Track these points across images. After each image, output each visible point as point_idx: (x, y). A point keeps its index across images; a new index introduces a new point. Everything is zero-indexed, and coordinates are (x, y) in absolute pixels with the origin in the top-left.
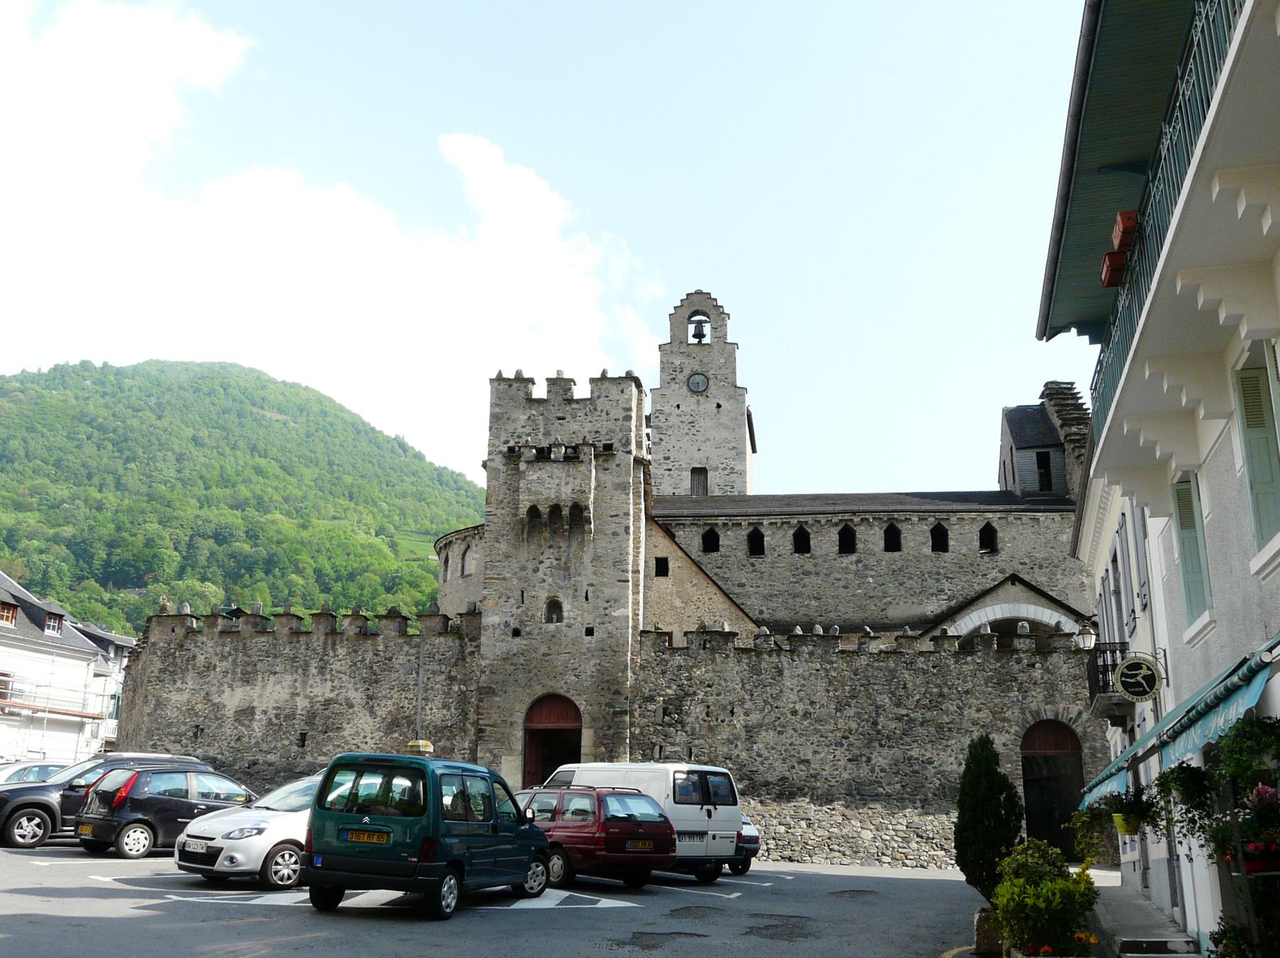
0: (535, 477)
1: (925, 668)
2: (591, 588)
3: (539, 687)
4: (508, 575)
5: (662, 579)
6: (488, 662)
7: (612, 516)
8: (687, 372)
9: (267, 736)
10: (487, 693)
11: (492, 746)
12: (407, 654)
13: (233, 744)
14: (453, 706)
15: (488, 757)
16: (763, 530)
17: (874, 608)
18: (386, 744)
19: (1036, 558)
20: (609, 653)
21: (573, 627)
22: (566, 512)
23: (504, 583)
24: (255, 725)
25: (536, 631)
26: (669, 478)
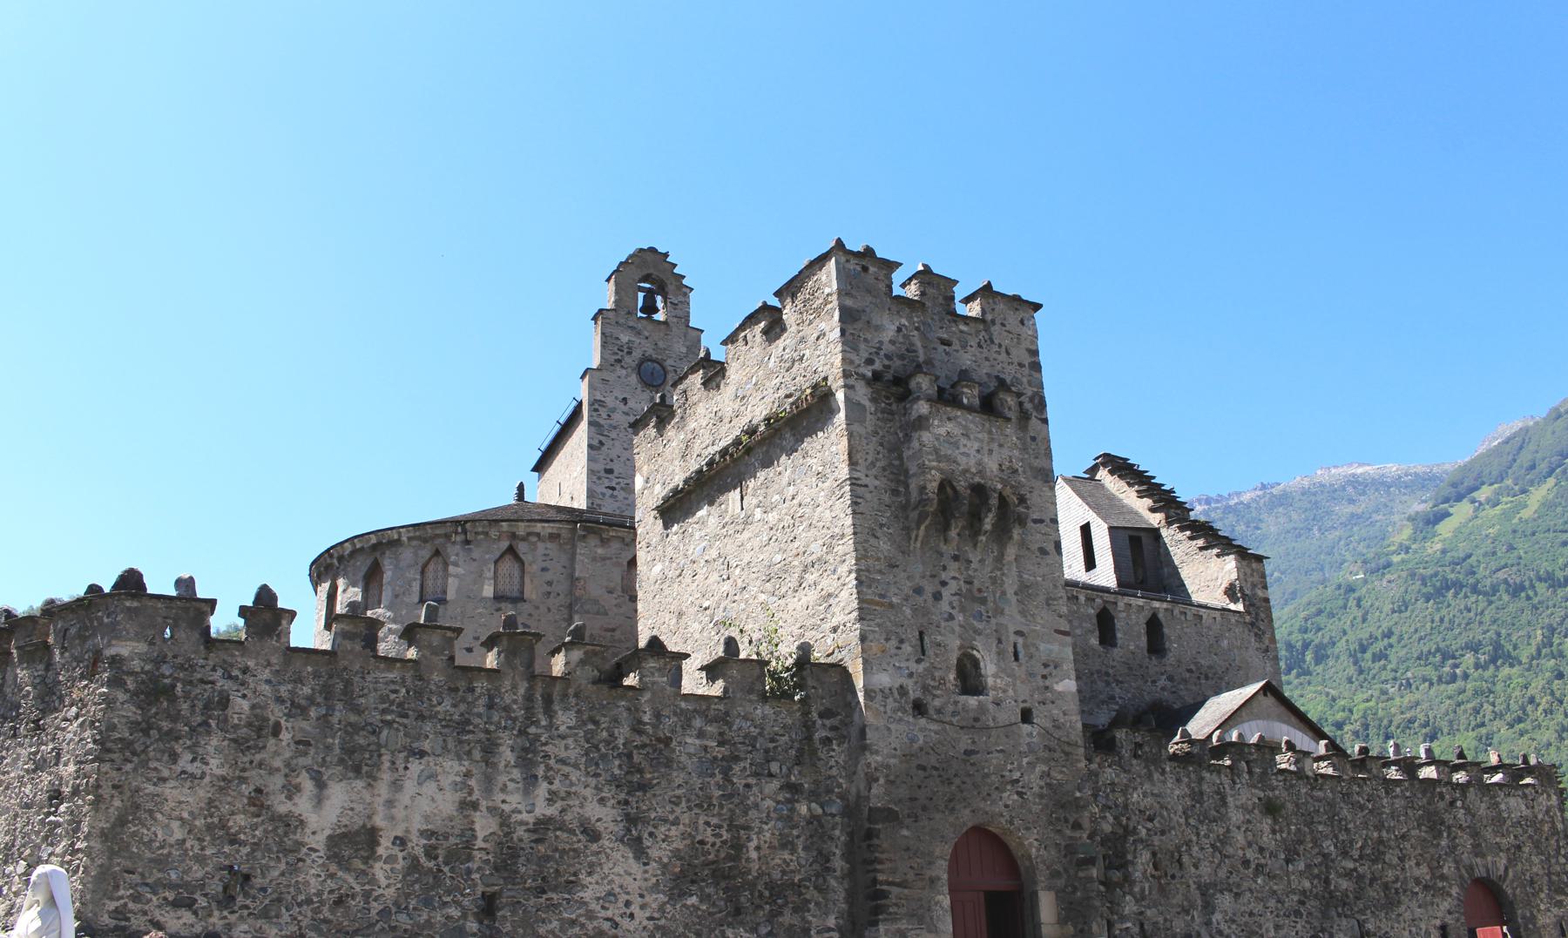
0: (942, 431)
2: (1020, 641)
4: (894, 600)
6: (879, 758)
8: (637, 354)
9: (407, 896)
12: (701, 734)
13: (326, 913)
14: (800, 844)
18: (673, 919)
21: (1003, 704)
24: (379, 871)
25: (951, 708)
26: (611, 500)
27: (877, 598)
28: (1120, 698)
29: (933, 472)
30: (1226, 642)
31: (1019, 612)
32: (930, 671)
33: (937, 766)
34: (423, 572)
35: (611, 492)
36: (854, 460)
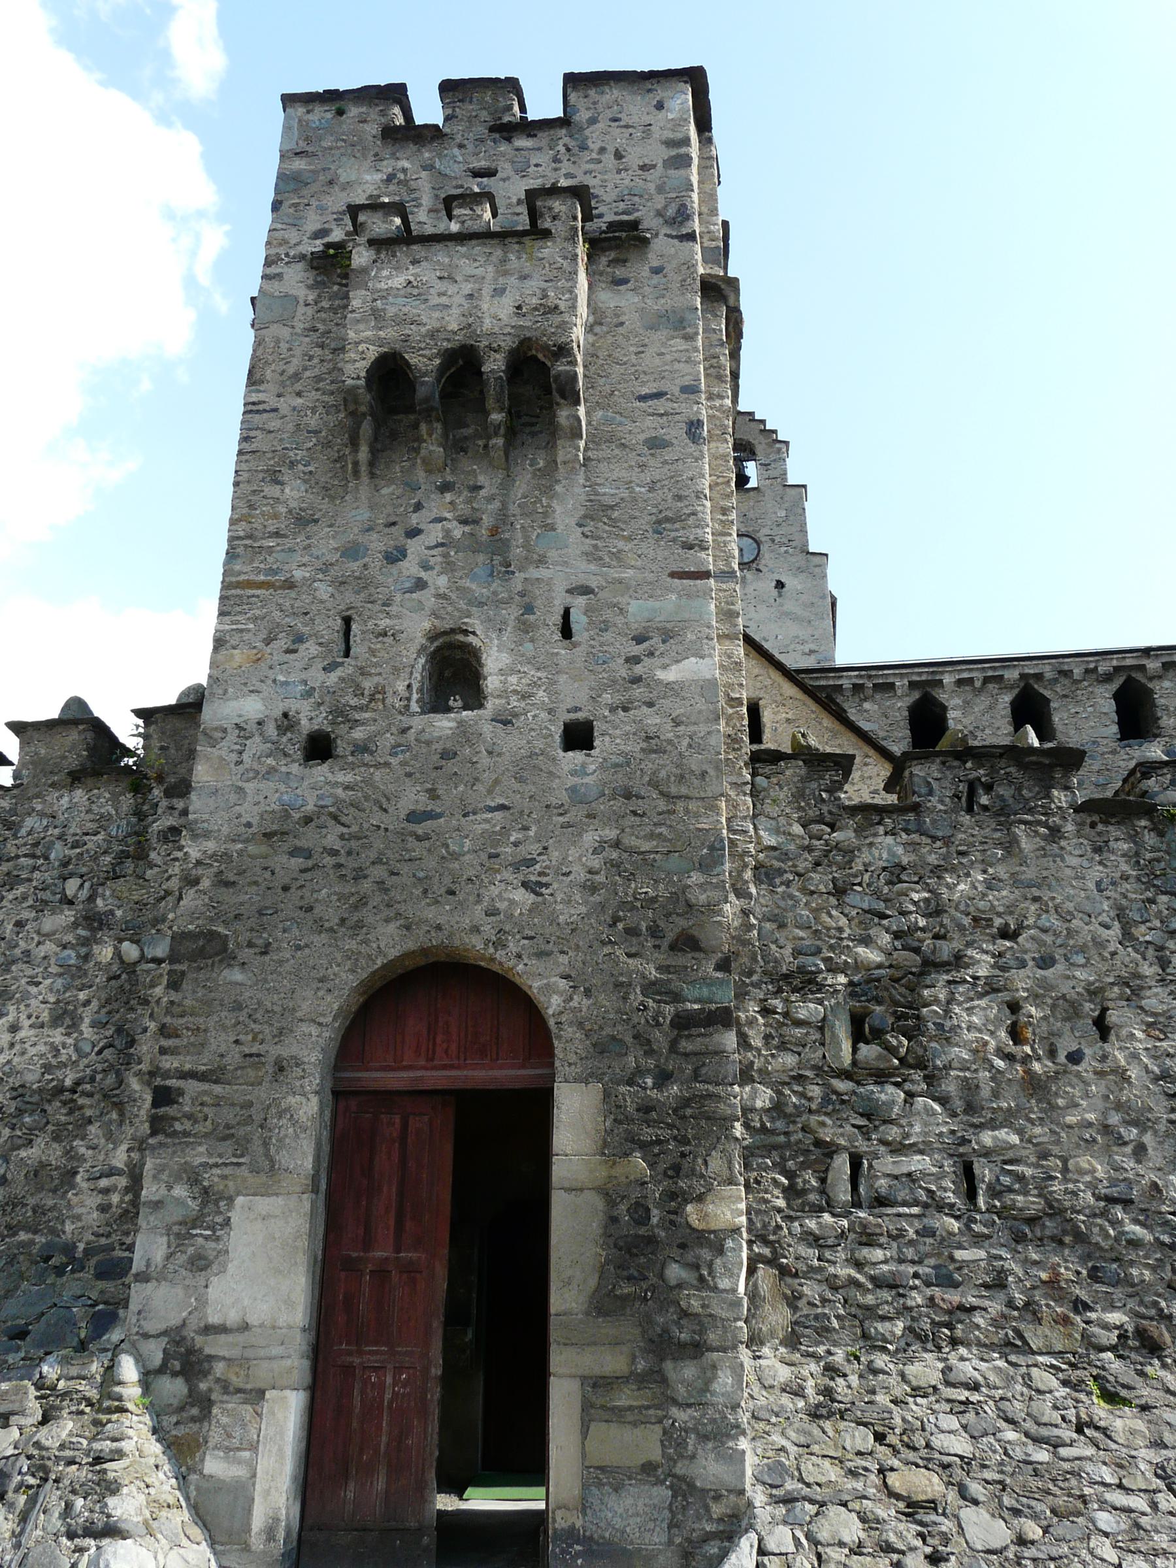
0: (398, 281)
2: (580, 602)
3: (392, 928)
4: (298, 574)
6: (211, 846)
7: (643, 398)
10: (201, 953)
11: (198, 1155)
15: (179, 1202)
16: (942, 697)
21: (518, 723)
22: (494, 365)
23: (286, 599)
25: (389, 739)
36: (258, 376)
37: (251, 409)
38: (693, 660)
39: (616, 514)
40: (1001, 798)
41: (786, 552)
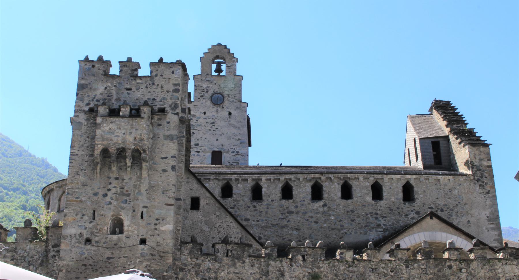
0: (107, 128)
1: (386, 272)
2: (145, 210)
4: (83, 199)
5: (195, 212)
6: (65, 262)
7: (163, 158)
8: (211, 92)
16: (261, 184)
17: (335, 236)
19: (439, 205)
20: (157, 257)
22: (129, 153)
25: (103, 240)
27: (75, 199)
28: (384, 225)
29: (99, 146)
30: (456, 191)
31: (147, 198)
32: (95, 227)
33: (92, 264)
34: (60, 200)
35: (197, 153)
36: (73, 145)
37: (72, 154)
38: (168, 225)
39: (154, 189)
40: (234, 254)
41: (233, 101)
